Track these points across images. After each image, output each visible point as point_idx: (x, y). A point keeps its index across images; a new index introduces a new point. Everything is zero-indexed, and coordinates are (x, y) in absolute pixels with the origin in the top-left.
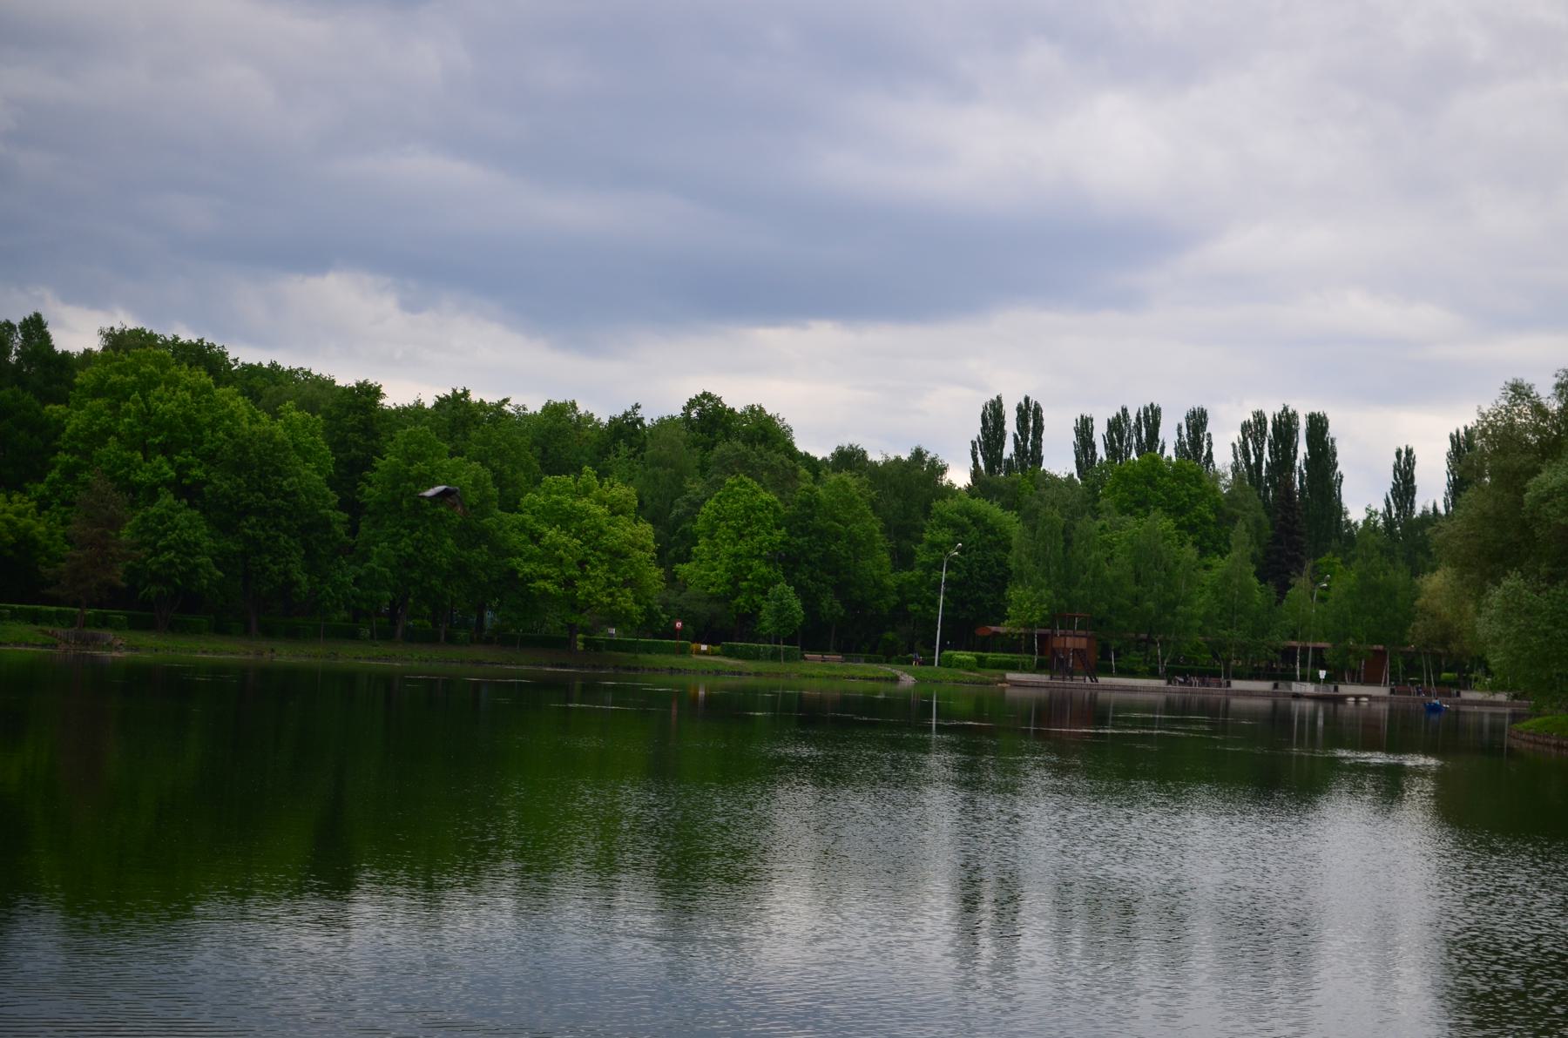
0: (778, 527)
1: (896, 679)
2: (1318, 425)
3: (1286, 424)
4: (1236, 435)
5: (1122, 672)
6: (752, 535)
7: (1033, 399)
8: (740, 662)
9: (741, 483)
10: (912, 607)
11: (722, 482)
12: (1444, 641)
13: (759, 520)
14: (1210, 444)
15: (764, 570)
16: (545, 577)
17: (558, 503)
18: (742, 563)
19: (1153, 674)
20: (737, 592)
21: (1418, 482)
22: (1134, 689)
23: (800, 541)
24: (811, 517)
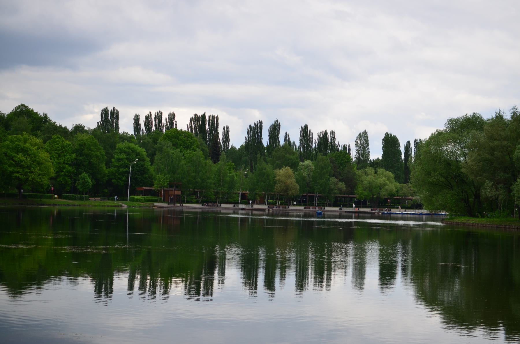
0: (73, 153)
1: (121, 206)
2: (333, 133)
3: (259, 126)
4: (144, 119)
5: (188, 202)
6: (64, 156)
7: (116, 108)
8: (65, 200)
9: (58, 137)
10: (113, 181)
11: (51, 137)
12: (286, 191)
13: (66, 151)
14: (176, 124)
15: (69, 168)
16: (18, 172)
17: (19, 145)
18: (61, 166)
19: (197, 203)
20: (58, 176)
21: (231, 137)
22: (195, 208)
23: (81, 158)
24: (83, 150)
